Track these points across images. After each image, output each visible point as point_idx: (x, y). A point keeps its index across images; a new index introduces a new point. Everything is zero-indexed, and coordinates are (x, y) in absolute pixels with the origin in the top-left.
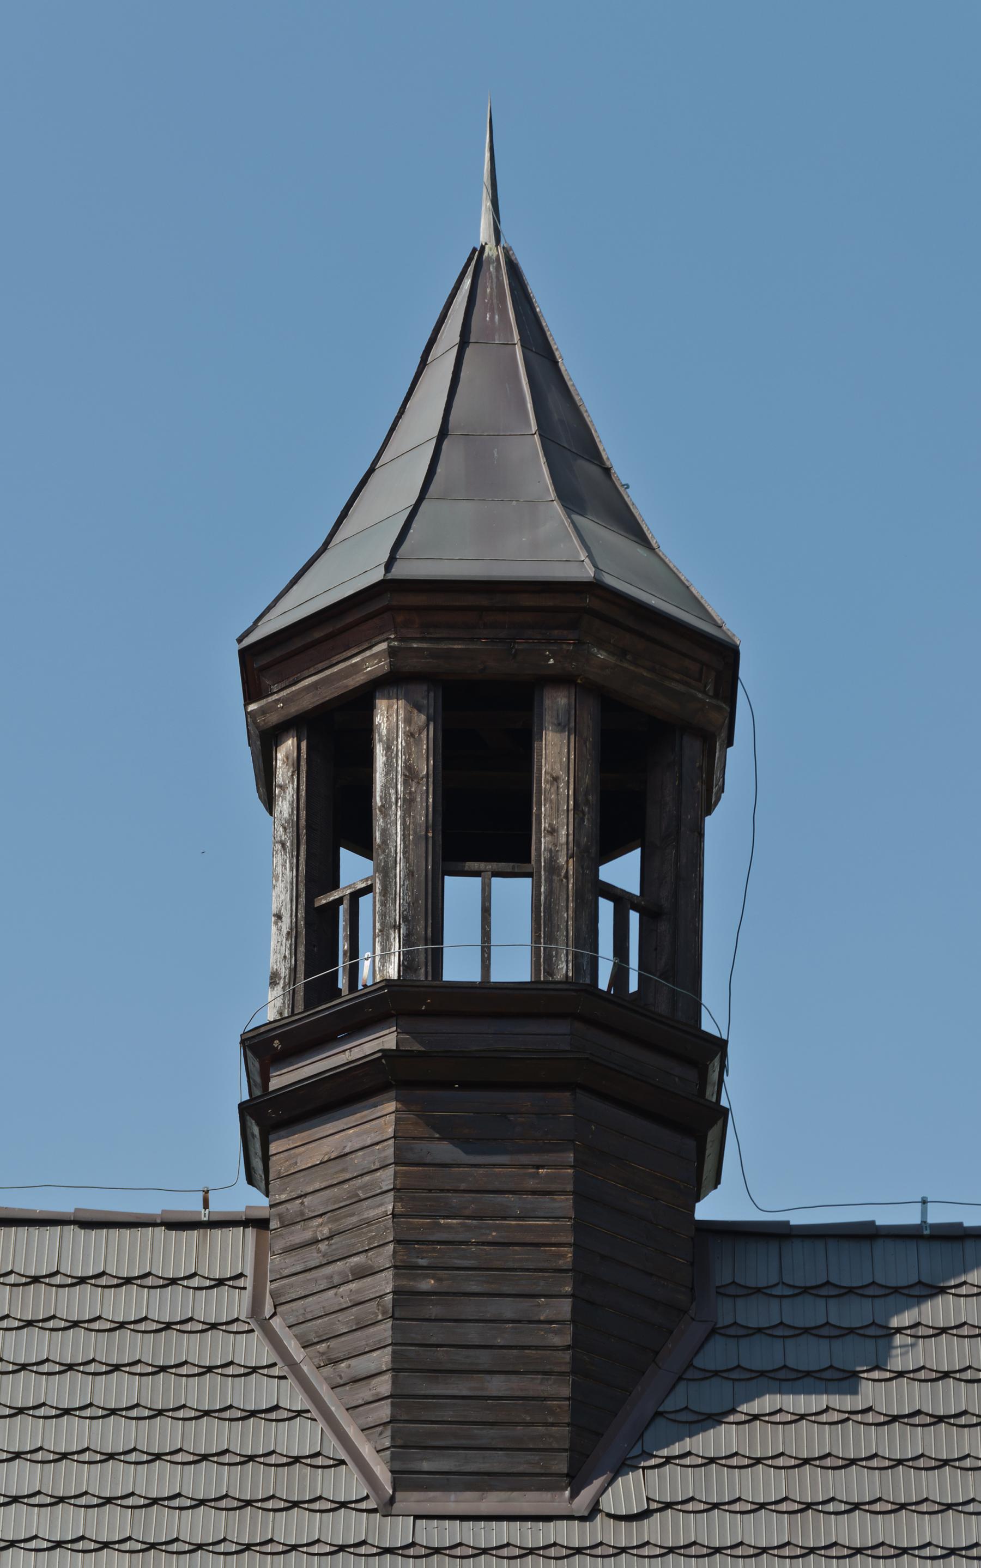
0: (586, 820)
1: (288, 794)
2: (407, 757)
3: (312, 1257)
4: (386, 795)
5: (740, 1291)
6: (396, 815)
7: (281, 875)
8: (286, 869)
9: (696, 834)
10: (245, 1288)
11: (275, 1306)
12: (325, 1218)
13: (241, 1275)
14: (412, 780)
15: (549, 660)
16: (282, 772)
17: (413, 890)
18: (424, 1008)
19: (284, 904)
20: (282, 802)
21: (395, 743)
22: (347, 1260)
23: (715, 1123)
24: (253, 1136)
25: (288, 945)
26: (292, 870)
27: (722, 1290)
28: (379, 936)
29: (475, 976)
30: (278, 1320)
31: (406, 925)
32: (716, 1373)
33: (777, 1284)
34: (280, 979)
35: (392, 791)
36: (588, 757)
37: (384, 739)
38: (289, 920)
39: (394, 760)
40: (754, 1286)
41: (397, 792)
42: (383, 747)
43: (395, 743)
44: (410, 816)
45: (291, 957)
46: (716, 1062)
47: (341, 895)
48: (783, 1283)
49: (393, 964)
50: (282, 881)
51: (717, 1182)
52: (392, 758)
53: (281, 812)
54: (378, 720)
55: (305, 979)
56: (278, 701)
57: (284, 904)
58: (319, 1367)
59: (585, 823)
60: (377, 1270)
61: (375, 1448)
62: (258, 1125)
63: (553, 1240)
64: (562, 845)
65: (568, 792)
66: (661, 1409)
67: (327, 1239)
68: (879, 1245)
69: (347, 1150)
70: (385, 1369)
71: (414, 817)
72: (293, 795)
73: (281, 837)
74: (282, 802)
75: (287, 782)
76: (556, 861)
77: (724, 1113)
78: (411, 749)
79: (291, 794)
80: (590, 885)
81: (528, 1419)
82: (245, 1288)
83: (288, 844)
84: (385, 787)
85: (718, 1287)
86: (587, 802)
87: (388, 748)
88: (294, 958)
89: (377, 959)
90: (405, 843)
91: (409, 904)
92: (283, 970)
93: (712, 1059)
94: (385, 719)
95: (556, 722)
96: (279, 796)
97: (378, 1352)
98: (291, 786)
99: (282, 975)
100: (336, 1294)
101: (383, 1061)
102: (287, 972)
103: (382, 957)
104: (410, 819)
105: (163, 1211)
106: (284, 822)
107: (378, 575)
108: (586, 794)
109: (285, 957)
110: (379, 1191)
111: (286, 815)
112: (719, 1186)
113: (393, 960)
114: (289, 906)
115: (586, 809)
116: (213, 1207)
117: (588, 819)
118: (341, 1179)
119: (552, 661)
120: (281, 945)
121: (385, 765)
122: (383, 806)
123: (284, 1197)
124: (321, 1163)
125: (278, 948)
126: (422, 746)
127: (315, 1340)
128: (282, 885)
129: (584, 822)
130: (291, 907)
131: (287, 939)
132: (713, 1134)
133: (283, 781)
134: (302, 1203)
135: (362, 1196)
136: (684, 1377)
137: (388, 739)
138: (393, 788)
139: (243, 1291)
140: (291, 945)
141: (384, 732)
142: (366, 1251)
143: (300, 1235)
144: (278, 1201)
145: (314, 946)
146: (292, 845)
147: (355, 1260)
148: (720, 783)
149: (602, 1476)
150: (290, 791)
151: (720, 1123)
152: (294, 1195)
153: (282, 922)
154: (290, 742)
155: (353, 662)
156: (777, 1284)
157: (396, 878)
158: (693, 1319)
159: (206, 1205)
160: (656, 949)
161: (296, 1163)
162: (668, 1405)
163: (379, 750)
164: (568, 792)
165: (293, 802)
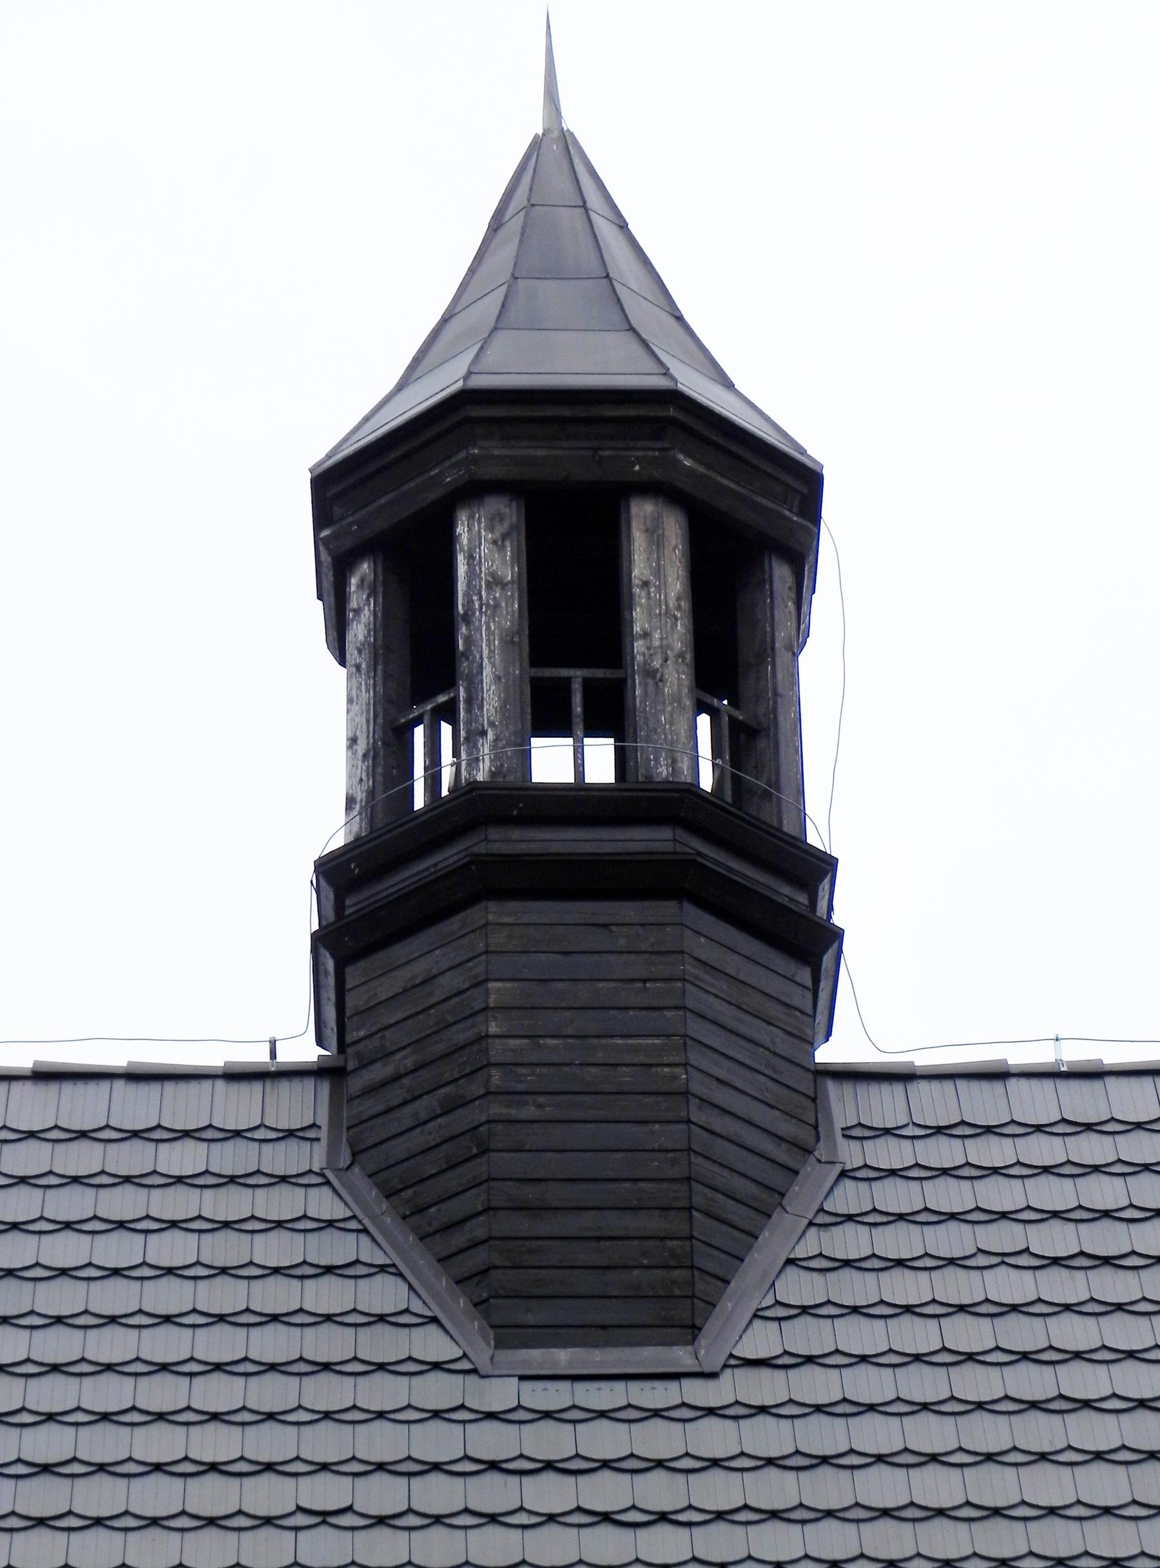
0: (679, 625)
1: (362, 616)
2: (490, 563)
3: (395, 1095)
4: (468, 602)
5: (867, 1133)
6: (480, 621)
7: (355, 699)
8: (361, 691)
9: (791, 653)
10: (318, 1140)
11: (354, 1155)
12: (408, 1050)
13: (314, 1126)
14: (496, 586)
15: (634, 466)
16: (356, 596)
17: (500, 695)
18: (515, 812)
19: (359, 726)
20: (357, 625)
21: (477, 550)
22: (436, 1092)
23: (833, 942)
24: (326, 973)
25: (364, 768)
26: (368, 691)
27: (847, 1133)
28: (464, 744)
29: (568, 777)
30: (356, 1170)
31: (492, 730)
32: (850, 1218)
33: (907, 1125)
34: (355, 804)
35: (475, 598)
36: (678, 564)
37: (466, 548)
38: (365, 742)
39: (477, 568)
40: (881, 1126)
41: (481, 598)
42: (464, 555)
43: (477, 550)
44: (494, 621)
45: (368, 779)
46: (827, 881)
47: (421, 712)
48: (914, 1124)
49: (481, 771)
50: (357, 704)
51: (829, 1034)
52: (475, 566)
53: (355, 635)
54: (459, 530)
55: (385, 792)
56: (352, 524)
57: (359, 726)
58: (404, 1218)
59: (679, 628)
60: (469, 1098)
61: (471, 1301)
62: (333, 956)
63: (665, 1060)
64: (655, 648)
65: (660, 596)
66: (792, 1256)
67: (412, 1072)
68: (1012, 1083)
69: (434, 971)
70: (481, 1209)
71: (499, 622)
72: (369, 617)
73: (356, 660)
74: (357, 625)
75: (362, 605)
76: (649, 664)
77: (835, 936)
78: (494, 556)
79: (367, 616)
80: (687, 690)
81: (645, 1262)
82: (318, 1140)
83: (363, 666)
84: (467, 595)
85: (843, 1129)
86: (679, 608)
87: (470, 557)
88: (371, 780)
89: (464, 764)
90: (490, 648)
91: (496, 709)
92: (359, 793)
93: (822, 880)
94: (466, 529)
95: (643, 528)
96: (353, 620)
97: (474, 1191)
98: (366, 608)
99: (359, 799)
100: (422, 1132)
101: (473, 867)
102: (364, 795)
103: (469, 765)
104: (494, 625)
105: (225, 1062)
106: (359, 645)
107: (460, 384)
108: (678, 599)
109: (361, 780)
110: (469, 1012)
111: (361, 637)
112: (830, 1038)
113: (481, 767)
114: (365, 727)
115: (679, 615)
116: (280, 1058)
117: (681, 625)
118: (427, 1004)
119: (637, 468)
120: (357, 768)
121: (467, 574)
122: (465, 614)
123: (362, 1033)
124: (404, 991)
125: (354, 771)
126: (506, 553)
127: (400, 1186)
128: (357, 708)
129: (677, 626)
130: (368, 728)
131: (363, 761)
132: (827, 959)
133: (358, 604)
134: (383, 1037)
135: (451, 1019)
136: (814, 1222)
137: (469, 549)
138: (476, 595)
139: (315, 1144)
140: (368, 767)
141: (465, 542)
142: (456, 1080)
143: (378, 1072)
144: (355, 1039)
145: (393, 768)
146: (368, 666)
147: (443, 1091)
148: (807, 621)
149: (826, 876)
150: (366, 615)
151: (835, 946)
152: (374, 1029)
153: (357, 744)
154: (365, 566)
155: (432, 474)
156: (907, 1125)
157: (482, 683)
158: (819, 1161)
159: (273, 1055)
160: (756, 767)
161: (376, 995)
162: (799, 1253)
163: (461, 559)
164: (660, 596)
165: (369, 624)
